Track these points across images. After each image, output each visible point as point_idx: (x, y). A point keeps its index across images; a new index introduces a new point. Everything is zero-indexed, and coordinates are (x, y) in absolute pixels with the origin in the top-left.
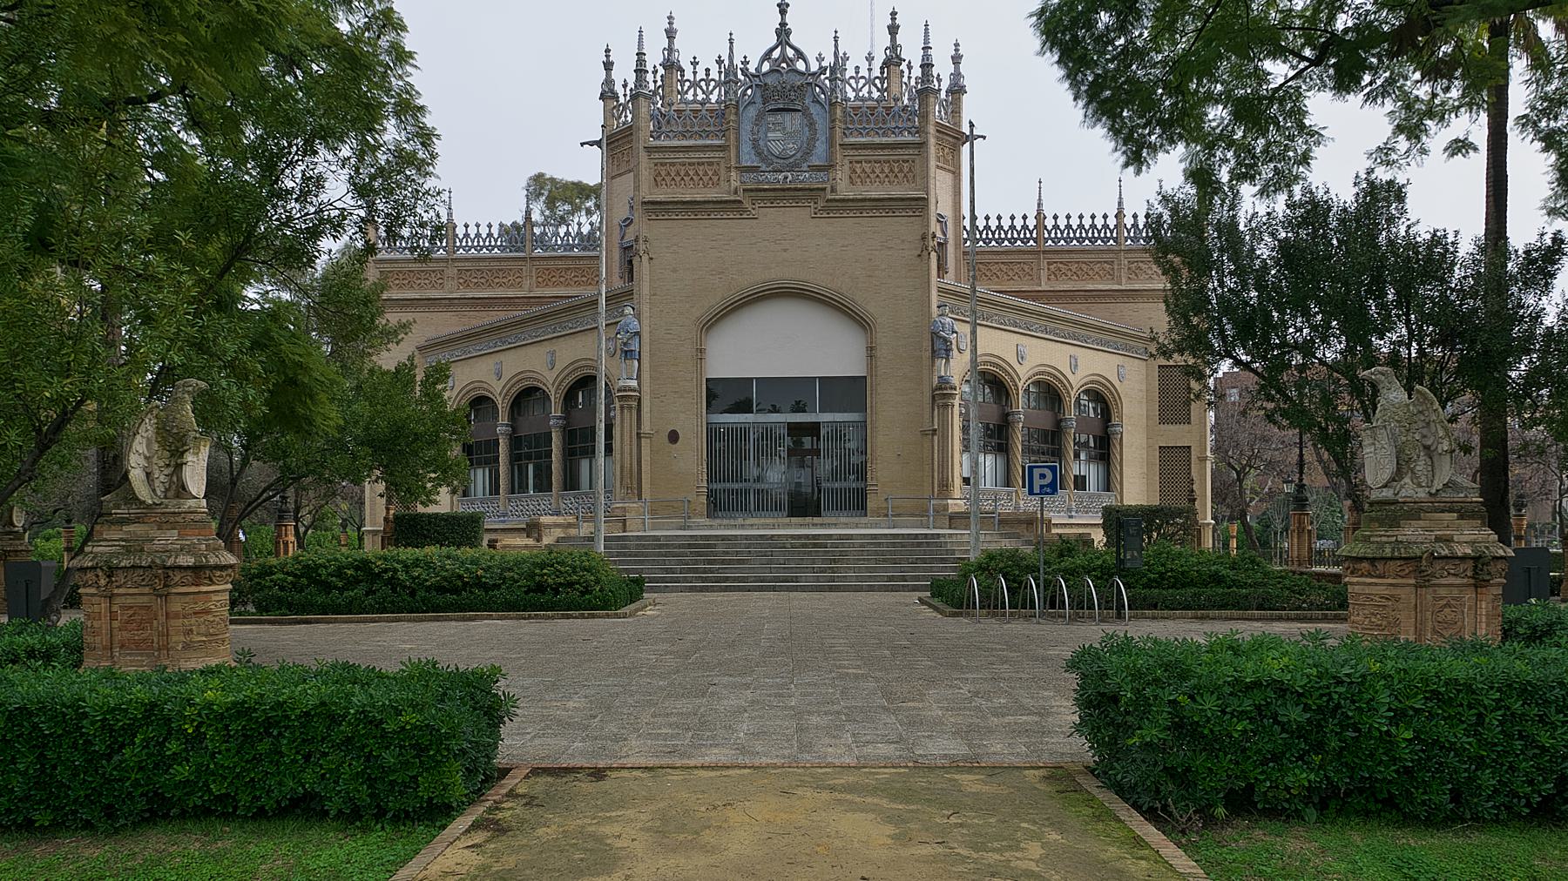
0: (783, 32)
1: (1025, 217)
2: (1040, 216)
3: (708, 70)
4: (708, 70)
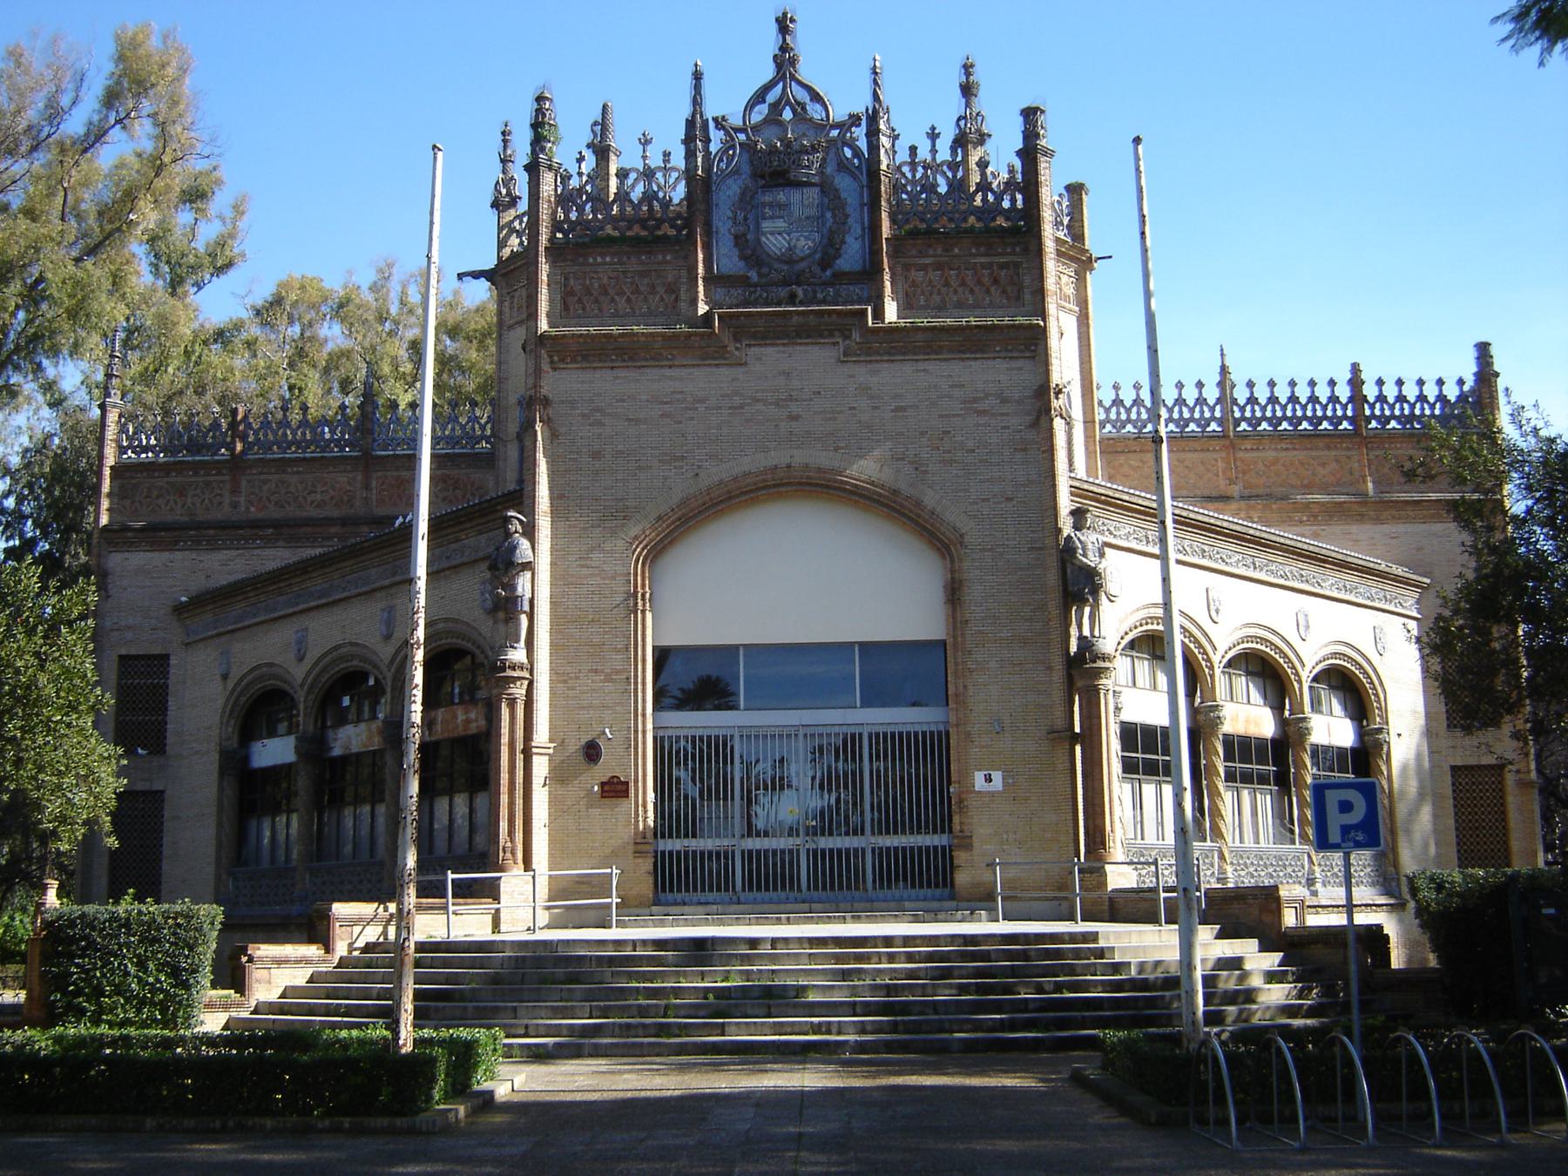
0: (785, 61)
1: (1200, 385)
2: (1356, 382)
3: (667, 155)
4: (667, 155)
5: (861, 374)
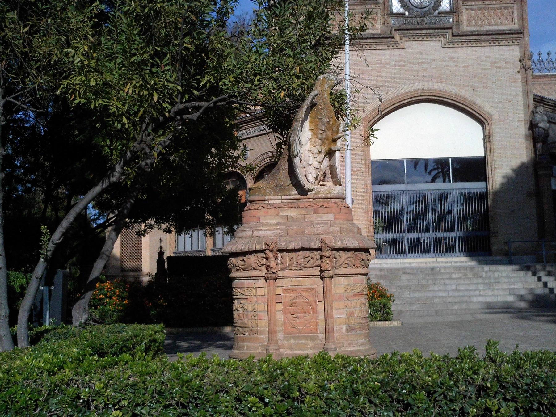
5: (450, 52)
